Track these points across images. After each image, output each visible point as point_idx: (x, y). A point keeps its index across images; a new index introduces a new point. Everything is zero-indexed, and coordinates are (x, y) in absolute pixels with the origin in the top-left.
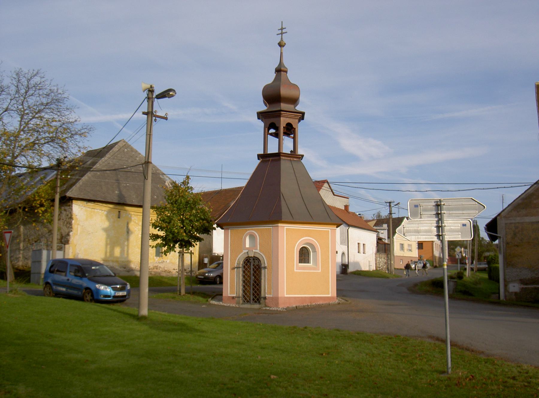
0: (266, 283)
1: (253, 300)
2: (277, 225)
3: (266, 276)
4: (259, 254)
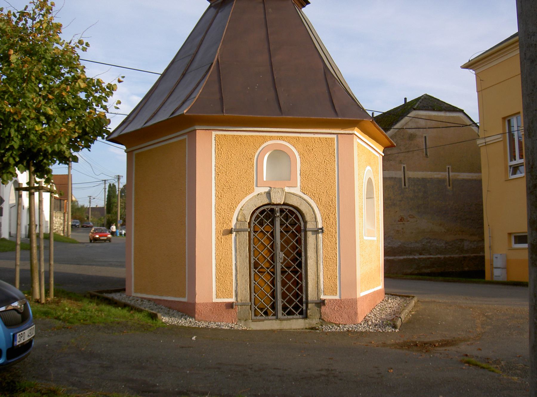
0: (321, 267)
1: (284, 308)
2: (351, 132)
3: (321, 252)
4: (300, 197)
